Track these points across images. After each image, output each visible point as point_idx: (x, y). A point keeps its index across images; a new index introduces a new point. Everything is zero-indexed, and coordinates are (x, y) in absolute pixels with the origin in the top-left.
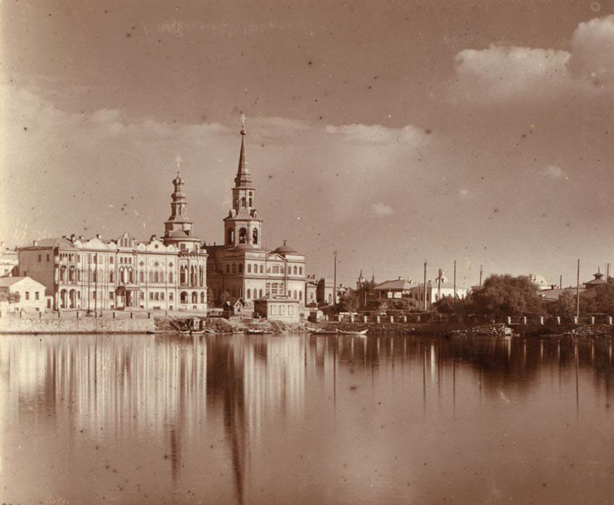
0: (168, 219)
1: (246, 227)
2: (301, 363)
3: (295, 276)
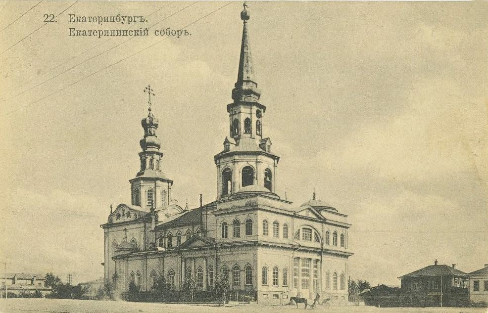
0: (136, 174)
1: (253, 164)
2: (260, 169)
3: (335, 248)
